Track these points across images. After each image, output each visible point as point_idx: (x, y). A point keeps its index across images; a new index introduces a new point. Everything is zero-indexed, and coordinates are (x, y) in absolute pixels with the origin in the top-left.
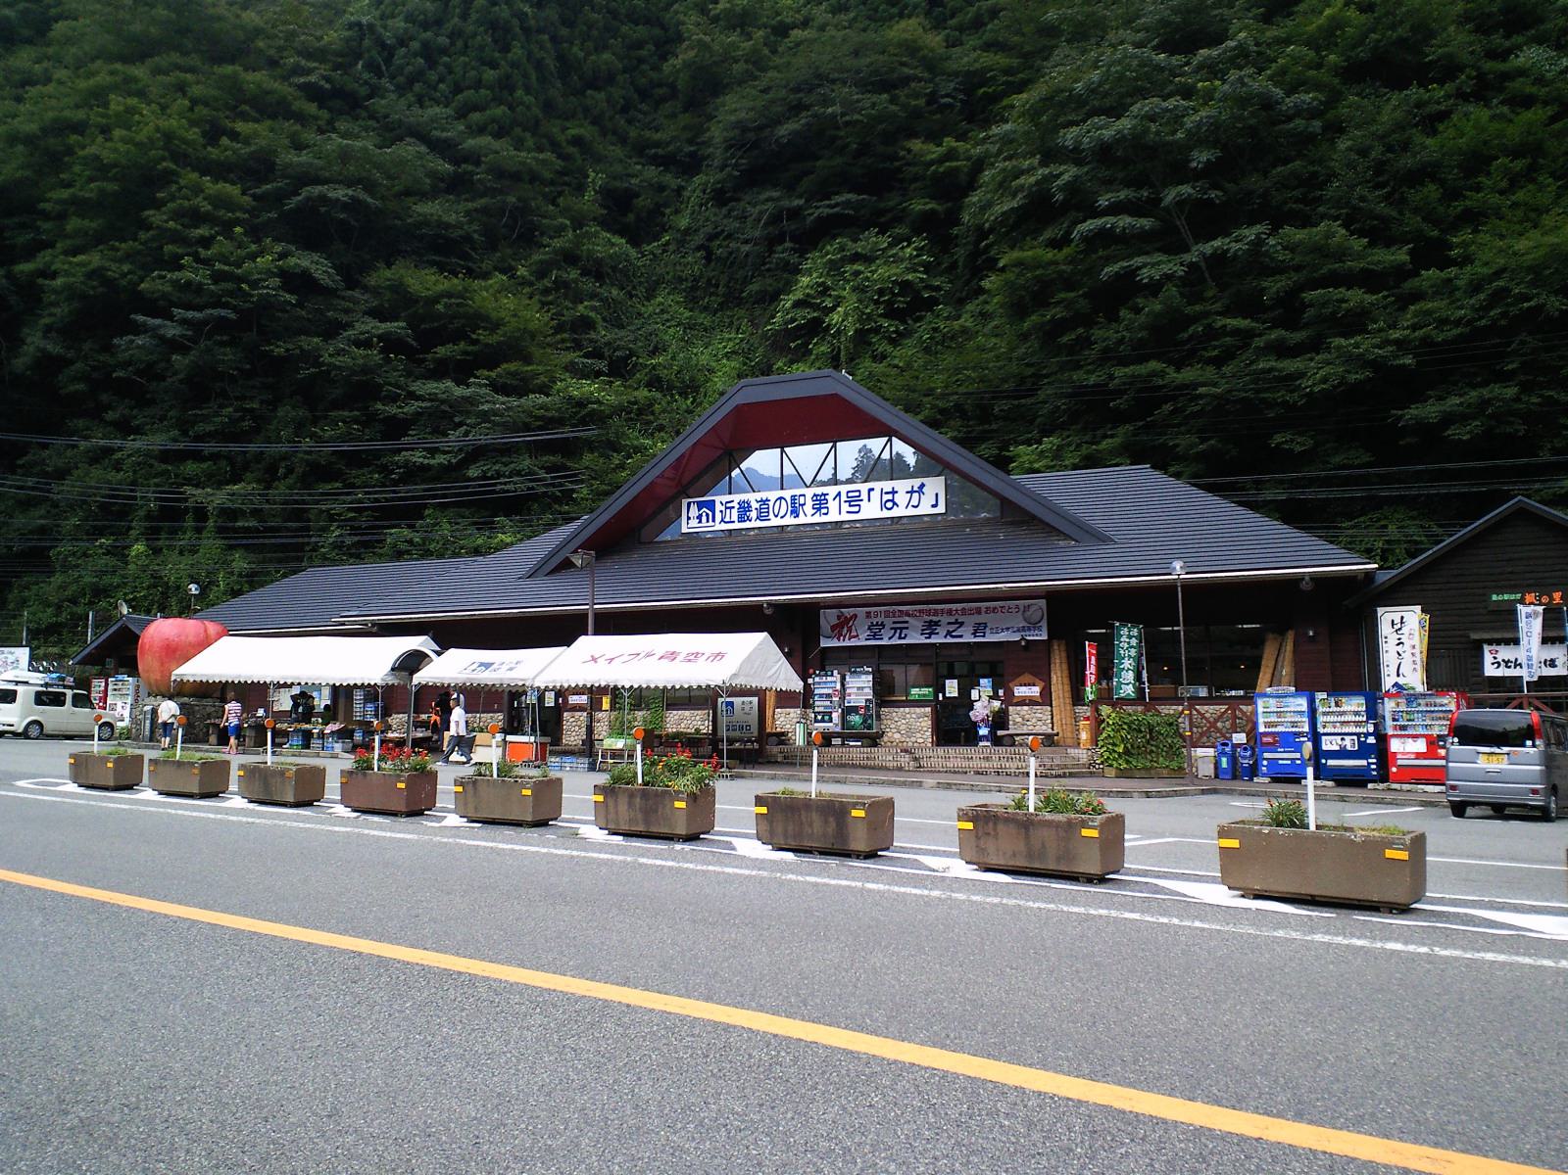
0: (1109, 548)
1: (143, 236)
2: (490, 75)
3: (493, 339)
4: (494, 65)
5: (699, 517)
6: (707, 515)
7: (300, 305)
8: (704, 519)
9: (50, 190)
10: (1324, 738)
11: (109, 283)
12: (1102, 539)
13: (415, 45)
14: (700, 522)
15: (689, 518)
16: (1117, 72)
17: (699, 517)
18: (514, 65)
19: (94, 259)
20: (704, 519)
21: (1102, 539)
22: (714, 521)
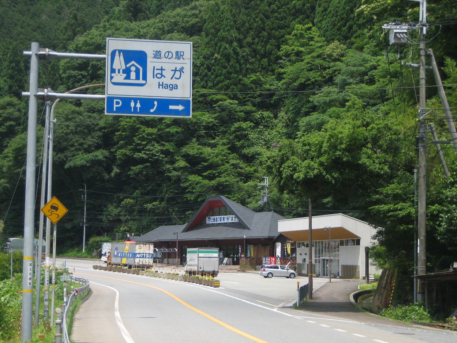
0: (249, 230)
1: (134, 144)
2: (224, 71)
3: (206, 164)
4: (225, 68)
5: (127, 71)
6: (137, 71)
7: (166, 157)
8: (133, 75)
9: (369, 292)
10: (313, 228)
11: (128, 156)
12: (249, 229)
13: (205, 66)
14: (128, 77)
15: (113, 71)
16: (339, 155)
17: (127, 71)
18: (232, 66)
19: (124, 151)
20: (133, 75)
21: (249, 229)
22: (145, 78)
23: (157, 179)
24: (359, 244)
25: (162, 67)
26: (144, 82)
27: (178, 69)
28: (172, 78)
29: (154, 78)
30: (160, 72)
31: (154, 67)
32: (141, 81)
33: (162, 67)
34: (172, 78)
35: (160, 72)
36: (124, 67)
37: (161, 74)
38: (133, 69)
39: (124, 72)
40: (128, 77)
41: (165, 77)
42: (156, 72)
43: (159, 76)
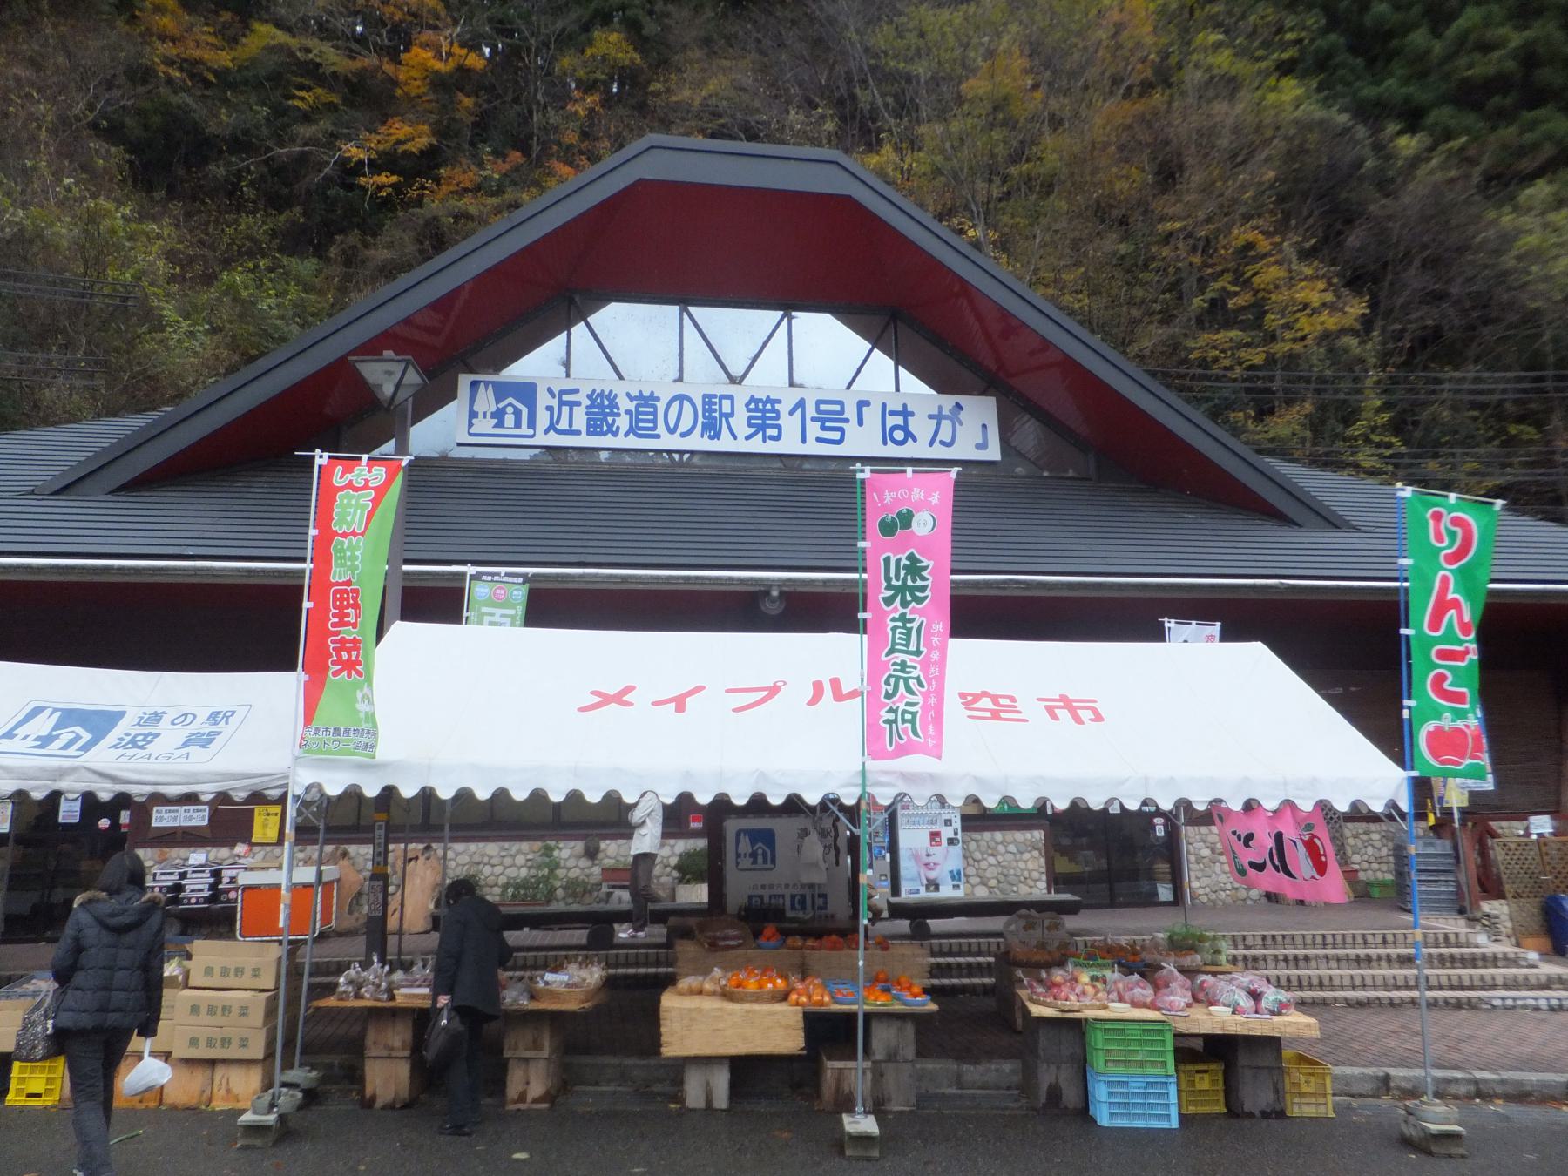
5: (499, 415)
14: (755, 862)
23: (1438, 48)
24: (1279, 1039)
25: (905, 406)
26: (531, 432)
27: (946, 412)
28: (931, 444)
29: (885, 443)
30: (899, 420)
31: (884, 405)
32: (525, 430)
33: (905, 406)
34: (931, 444)
35: (899, 420)
36: (494, 409)
37: (905, 428)
38: (510, 410)
39: (493, 415)
40: (755, 862)
41: (915, 440)
42: (891, 421)
43: (899, 435)
